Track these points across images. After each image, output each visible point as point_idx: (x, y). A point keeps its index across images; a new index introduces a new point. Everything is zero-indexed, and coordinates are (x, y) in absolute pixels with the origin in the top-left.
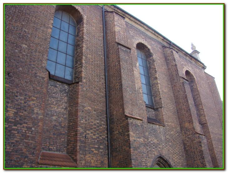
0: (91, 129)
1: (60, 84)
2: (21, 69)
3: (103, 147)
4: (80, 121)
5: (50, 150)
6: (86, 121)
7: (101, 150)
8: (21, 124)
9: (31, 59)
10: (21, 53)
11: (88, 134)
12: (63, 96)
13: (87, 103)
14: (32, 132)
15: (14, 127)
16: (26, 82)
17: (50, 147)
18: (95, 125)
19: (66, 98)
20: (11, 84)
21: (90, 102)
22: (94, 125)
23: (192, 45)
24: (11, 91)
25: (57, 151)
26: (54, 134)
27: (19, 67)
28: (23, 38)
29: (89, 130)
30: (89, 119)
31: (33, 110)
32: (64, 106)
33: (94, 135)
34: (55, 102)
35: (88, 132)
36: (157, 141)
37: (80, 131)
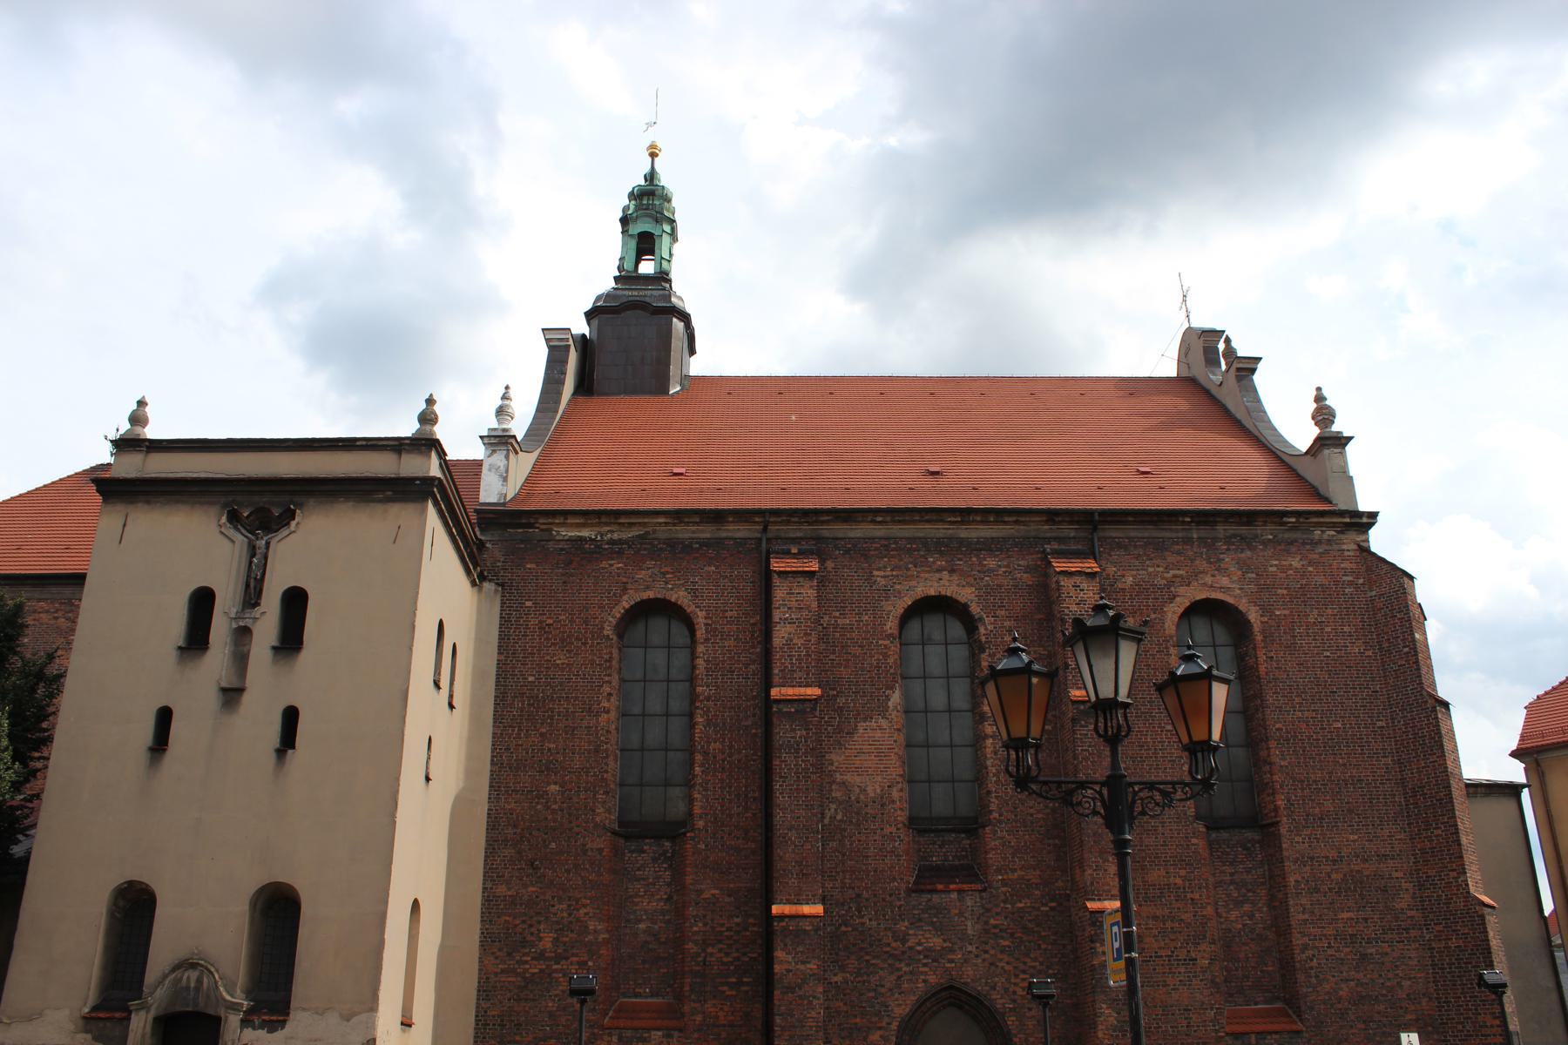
0: (720, 941)
1: (652, 841)
2: (553, 845)
3: (750, 980)
4: (691, 927)
5: (636, 995)
6: (705, 925)
7: (745, 988)
8: (567, 958)
9: (570, 815)
10: (548, 808)
11: (712, 954)
12: (660, 871)
13: (709, 881)
14: (588, 969)
15: (555, 967)
16: (566, 870)
17: (637, 990)
18: (729, 929)
19: (667, 873)
20: (539, 885)
21: (716, 875)
22: (727, 931)
23: (1320, 398)
24: (542, 897)
25: (652, 996)
26: (644, 962)
27: (549, 844)
28: (548, 769)
29: (713, 946)
30: (712, 920)
31: (587, 927)
32: (662, 893)
33: (727, 954)
34: (642, 890)
35: (710, 950)
36: (944, 941)
37: (692, 951)
